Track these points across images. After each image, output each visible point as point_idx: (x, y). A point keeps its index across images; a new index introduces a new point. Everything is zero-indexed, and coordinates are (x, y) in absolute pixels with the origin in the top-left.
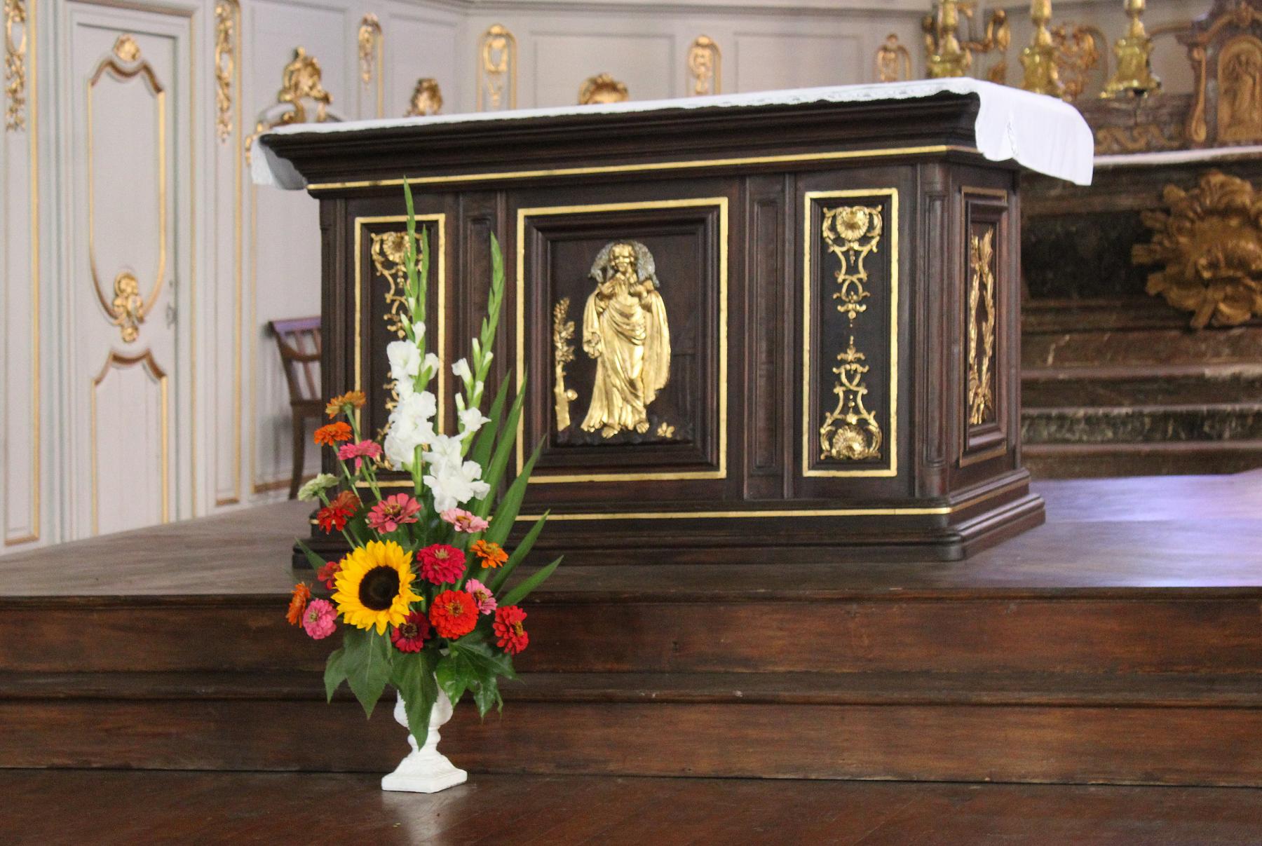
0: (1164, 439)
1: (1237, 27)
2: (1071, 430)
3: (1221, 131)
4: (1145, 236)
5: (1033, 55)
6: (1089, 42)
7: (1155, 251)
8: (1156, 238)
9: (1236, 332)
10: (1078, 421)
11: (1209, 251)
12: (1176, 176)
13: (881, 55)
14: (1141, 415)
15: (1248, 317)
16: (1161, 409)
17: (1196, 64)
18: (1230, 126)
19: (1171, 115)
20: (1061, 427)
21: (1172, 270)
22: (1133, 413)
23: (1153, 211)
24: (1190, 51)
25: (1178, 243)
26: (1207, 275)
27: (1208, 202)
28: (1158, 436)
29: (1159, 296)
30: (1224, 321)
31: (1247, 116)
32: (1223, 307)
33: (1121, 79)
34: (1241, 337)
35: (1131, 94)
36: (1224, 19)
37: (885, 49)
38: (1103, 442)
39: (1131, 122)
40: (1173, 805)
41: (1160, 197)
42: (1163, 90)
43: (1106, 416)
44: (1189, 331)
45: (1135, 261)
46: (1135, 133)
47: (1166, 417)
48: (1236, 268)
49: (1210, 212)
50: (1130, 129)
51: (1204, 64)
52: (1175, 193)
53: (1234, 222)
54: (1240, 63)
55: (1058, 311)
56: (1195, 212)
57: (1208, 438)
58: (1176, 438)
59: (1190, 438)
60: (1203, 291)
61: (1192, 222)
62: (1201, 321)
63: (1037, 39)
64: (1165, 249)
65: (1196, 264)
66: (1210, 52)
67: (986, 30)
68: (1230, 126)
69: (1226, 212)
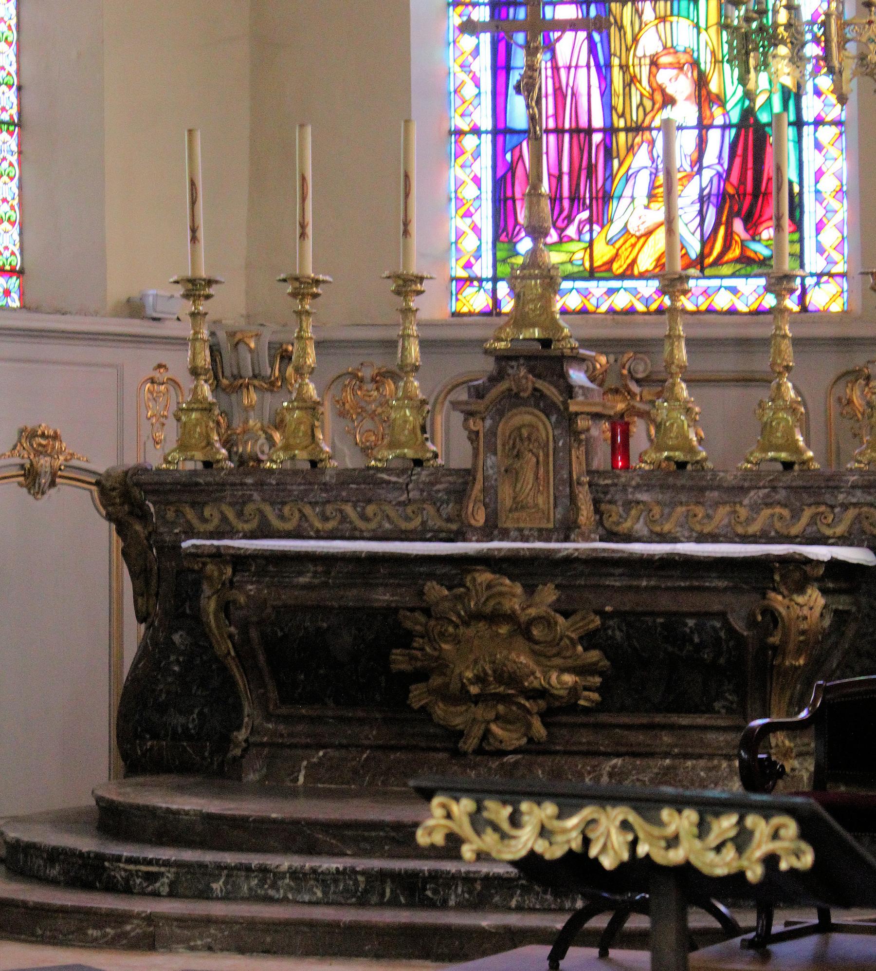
0: (382, 904)
1: (517, 395)
2: (274, 886)
3: (502, 516)
4: (405, 639)
7: (416, 659)
8: (418, 642)
9: (511, 758)
10: (282, 875)
11: (476, 662)
12: (441, 570)
13: (148, 385)
14: (354, 871)
15: (524, 741)
16: (376, 864)
17: (474, 437)
18: (511, 511)
19: (448, 492)
20: (263, 881)
21: (436, 681)
22: (345, 869)
23: (412, 610)
24: (466, 420)
25: (441, 649)
26: (474, 690)
28: (374, 899)
29: (423, 709)
30: (495, 745)
31: (530, 500)
32: (494, 727)
33: (392, 446)
34: (516, 763)
36: (503, 386)
37: (153, 381)
38: (310, 903)
39: (403, 498)
41: (421, 594)
42: (440, 461)
43: (314, 871)
44: (457, 753)
45: (395, 667)
46: (409, 510)
47: (383, 875)
48: (508, 685)
49: (477, 616)
50: (399, 504)
51: (481, 435)
52: (435, 591)
53: (503, 630)
54: (521, 440)
55: (312, 720)
56: (459, 616)
57: (430, 905)
58: (394, 903)
59: (410, 905)
60: (473, 708)
61: (456, 626)
62: (470, 744)
64: (426, 654)
65: (461, 676)
68: (511, 511)
69: (495, 617)
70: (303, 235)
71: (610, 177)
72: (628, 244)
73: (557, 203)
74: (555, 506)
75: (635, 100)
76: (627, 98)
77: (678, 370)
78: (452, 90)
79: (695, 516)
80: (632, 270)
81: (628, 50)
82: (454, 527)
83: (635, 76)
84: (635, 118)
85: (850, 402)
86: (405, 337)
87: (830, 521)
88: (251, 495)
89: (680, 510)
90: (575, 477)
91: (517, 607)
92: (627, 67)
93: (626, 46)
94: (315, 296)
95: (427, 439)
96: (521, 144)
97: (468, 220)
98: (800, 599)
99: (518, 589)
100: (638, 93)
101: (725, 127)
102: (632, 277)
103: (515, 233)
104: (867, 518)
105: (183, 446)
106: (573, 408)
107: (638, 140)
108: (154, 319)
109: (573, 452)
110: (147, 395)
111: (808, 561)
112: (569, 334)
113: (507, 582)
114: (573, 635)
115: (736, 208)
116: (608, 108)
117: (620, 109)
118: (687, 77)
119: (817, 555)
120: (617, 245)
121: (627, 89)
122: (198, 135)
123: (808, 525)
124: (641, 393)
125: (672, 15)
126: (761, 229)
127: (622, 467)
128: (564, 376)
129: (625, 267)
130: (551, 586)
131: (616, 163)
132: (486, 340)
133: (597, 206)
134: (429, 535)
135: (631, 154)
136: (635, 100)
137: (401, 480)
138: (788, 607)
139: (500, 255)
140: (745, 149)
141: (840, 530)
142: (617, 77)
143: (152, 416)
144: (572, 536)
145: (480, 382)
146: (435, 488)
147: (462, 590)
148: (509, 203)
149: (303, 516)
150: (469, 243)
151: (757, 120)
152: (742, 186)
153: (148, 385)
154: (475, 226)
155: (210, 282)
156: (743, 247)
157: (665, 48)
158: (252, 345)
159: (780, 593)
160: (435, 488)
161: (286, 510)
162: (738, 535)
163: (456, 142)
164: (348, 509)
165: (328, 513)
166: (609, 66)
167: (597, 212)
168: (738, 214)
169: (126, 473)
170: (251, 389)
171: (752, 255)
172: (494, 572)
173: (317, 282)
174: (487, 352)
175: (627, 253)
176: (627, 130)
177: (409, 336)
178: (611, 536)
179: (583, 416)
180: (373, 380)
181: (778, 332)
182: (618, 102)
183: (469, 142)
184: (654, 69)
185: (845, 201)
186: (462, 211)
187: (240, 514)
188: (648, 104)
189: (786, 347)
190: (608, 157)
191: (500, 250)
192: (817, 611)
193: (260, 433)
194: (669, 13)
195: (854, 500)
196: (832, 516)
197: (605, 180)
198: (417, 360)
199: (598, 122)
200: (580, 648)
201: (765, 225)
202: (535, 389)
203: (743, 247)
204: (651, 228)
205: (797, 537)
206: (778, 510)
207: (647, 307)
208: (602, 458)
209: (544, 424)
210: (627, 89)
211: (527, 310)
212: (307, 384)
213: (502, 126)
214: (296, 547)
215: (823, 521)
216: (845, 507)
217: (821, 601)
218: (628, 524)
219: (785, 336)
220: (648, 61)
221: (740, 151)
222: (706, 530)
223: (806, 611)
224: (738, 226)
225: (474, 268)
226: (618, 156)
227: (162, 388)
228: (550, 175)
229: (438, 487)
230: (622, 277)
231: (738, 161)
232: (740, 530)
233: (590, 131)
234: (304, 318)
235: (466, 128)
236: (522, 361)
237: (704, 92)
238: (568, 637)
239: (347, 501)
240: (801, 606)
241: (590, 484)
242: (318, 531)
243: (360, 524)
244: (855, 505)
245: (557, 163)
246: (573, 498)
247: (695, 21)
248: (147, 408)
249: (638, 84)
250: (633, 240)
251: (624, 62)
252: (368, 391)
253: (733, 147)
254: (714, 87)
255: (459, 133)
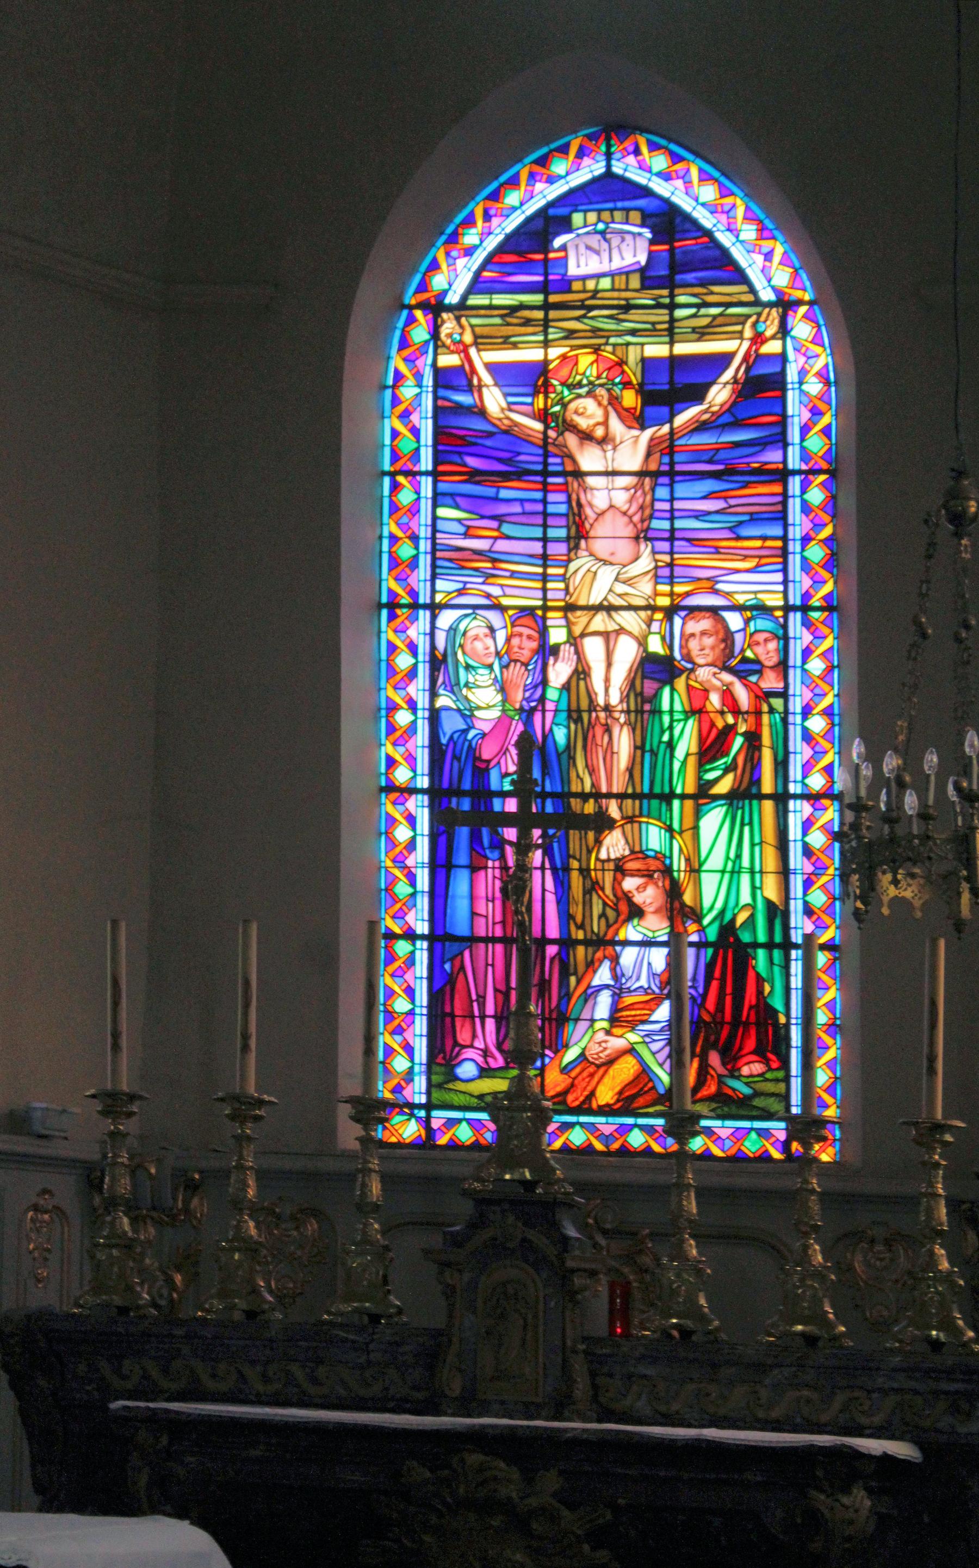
5: (233, 1250)
6: (312, 1227)
13: (31, 1214)
18: (492, 1379)
24: (441, 1273)
27: (461, 1491)
33: (348, 1299)
35: (366, 1319)
36: (487, 1234)
37: (36, 1208)
39: (363, 1359)
40: (799, 1355)
52: (418, 1472)
63: (238, 1228)
66: (466, 1277)
67: (175, 1199)
68: (492, 1379)
70: (245, 1048)
71: (566, 995)
72: (585, 1074)
73: (504, 1023)
74: (546, 1376)
75: (597, 908)
76: (587, 908)
77: (686, 1224)
78: (383, 886)
79: (708, 1395)
80: (590, 1103)
81: (589, 852)
82: (420, 1395)
83: (597, 882)
84: (596, 930)
85: (851, 1268)
86: (367, 1172)
87: (866, 1408)
88: (179, 1350)
89: (691, 1387)
90: (569, 1343)
91: (514, 1495)
92: (588, 870)
93: (587, 846)
94: (258, 1119)
95: (389, 1291)
96: (461, 953)
97: (399, 1038)
98: (845, 1500)
99: (515, 1474)
100: (600, 902)
101: (701, 945)
102: (590, 1112)
103: (454, 1054)
104: (910, 1406)
105: (97, 1289)
106: (570, 1264)
107: (599, 954)
108: (41, 1137)
109: (568, 1313)
110: (29, 1225)
111: (857, 1455)
112: (562, 1176)
113: (502, 1465)
114: (579, 1532)
115: (712, 1038)
116: (566, 917)
117: (579, 918)
118: (658, 886)
119: (868, 1448)
120: (573, 1074)
121: (588, 896)
122: (123, 925)
123: (841, 1411)
124: (608, 1245)
125: (641, 815)
126: (741, 1064)
127: (621, 1336)
128: (555, 1225)
129: (582, 1099)
130: (553, 1473)
131: (573, 980)
132: (465, 1179)
133: (550, 1030)
134: (391, 1405)
135: (590, 970)
136: (597, 908)
137: (361, 1339)
138: (832, 1509)
139: (436, 1079)
140: (724, 973)
141: (877, 1420)
142: (576, 880)
143: (34, 1249)
144: (566, 1413)
145: (458, 1228)
146: (400, 1350)
147: (446, 1472)
148: (448, 1020)
149: (241, 1375)
150: (400, 1064)
151: (738, 939)
152: (719, 1015)
153: (31, 1214)
154: (408, 1044)
155: (132, 1098)
156: (721, 1083)
157: (632, 852)
158: (153, 1171)
159: (822, 1491)
160: (400, 1350)
161: (222, 1366)
162: (758, 1420)
163: (386, 947)
164: (295, 1369)
165: (271, 1373)
166: (567, 869)
167: (551, 1035)
168: (714, 1046)
169: (28, 1317)
170: (149, 1221)
171: (730, 1092)
172: (486, 1454)
173: (261, 1103)
174: (465, 1193)
175: (584, 1084)
176: (586, 943)
177: (371, 1170)
178: (607, 1415)
179: (580, 1273)
180: (293, 1218)
181: (804, 1186)
182: (577, 911)
183: (402, 947)
184: (619, 875)
185: (838, 1037)
186: (391, 1027)
187: (165, 1371)
188: (611, 914)
189: (814, 1204)
190: (565, 973)
191: (436, 1074)
192: (864, 1513)
193: (158, 1273)
194: (637, 813)
195: (895, 1385)
196: (868, 1403)
197: (560, 998)
198: (378, 1198)
199: (553, 931)
200: (586, 1547)
201: (745, 1060)
202: (524, 1240)
203: (721, 1083)
204: (613, 1056)
205: (825, 1425)
206: (806, 1393)
207: (607, 1147)
208: (598, 1323)
209: (533, 1281)
210: (588, 896)
211: (512, 1147)
212: (246, 1222)
213: (440, 932)
214: (250, 1413)
215: (859, 1408)
216: (884, 1392)
217: (868, 1503)
218: (627, 1402)
219: (813, 1191)
220: (611, 866)
221: (717, 974)
222: (722, 1412)
223: (850, 1515)
224: (714, 1059)
225: (405, 1093)
226: (575, 973)
227: (46, 1217)
228: (496, 990)
229: (406, 1348)
230: (577, 1111)
231: (715, 984)
232: (761, 1414)
233: (543, 941)
234: (244, 1144)
235: (397, 930)
236: (507, 1206)
237: (677, 904)
238: (573, 1533)
239: (295, 1360)
240: (847, 1508)
241: (586, 1352)
242: (258, 1395)
243: (312, 1390)
244: (897, 1391)
245: (504, 976)
246: (565, 1367)
247: (668, 823)
248: (29, 1240)
249: (600, 893)
250: (591, 1069)
251: (584, 866)
252: (286, 1230)
253: (710, 967)
254: (688, 898)
255: (391, 936)
